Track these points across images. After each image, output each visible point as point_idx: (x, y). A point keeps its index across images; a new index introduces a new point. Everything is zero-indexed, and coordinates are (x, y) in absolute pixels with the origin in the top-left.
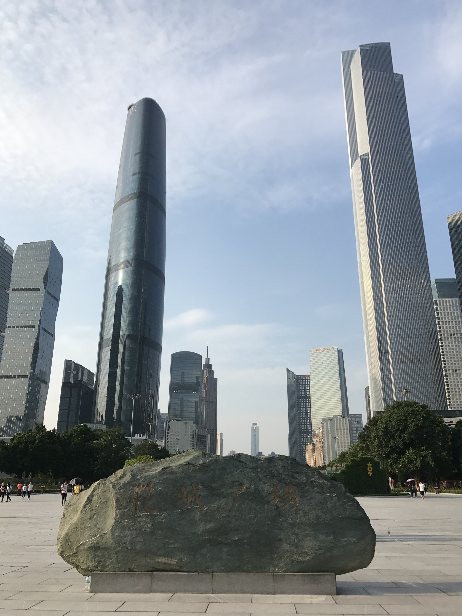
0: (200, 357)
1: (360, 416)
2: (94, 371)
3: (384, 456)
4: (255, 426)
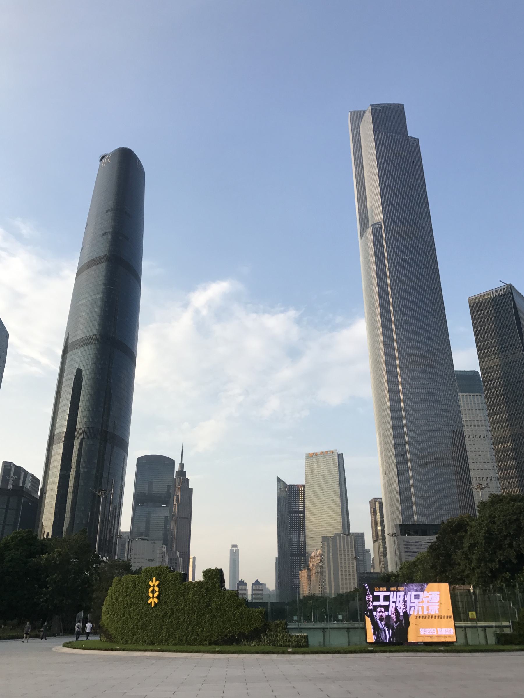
0: (172, 462)
1: (362, 535)
2: (40, 476)
3: (490, 575)
4: (235, 549)
